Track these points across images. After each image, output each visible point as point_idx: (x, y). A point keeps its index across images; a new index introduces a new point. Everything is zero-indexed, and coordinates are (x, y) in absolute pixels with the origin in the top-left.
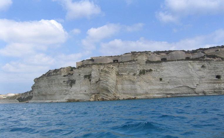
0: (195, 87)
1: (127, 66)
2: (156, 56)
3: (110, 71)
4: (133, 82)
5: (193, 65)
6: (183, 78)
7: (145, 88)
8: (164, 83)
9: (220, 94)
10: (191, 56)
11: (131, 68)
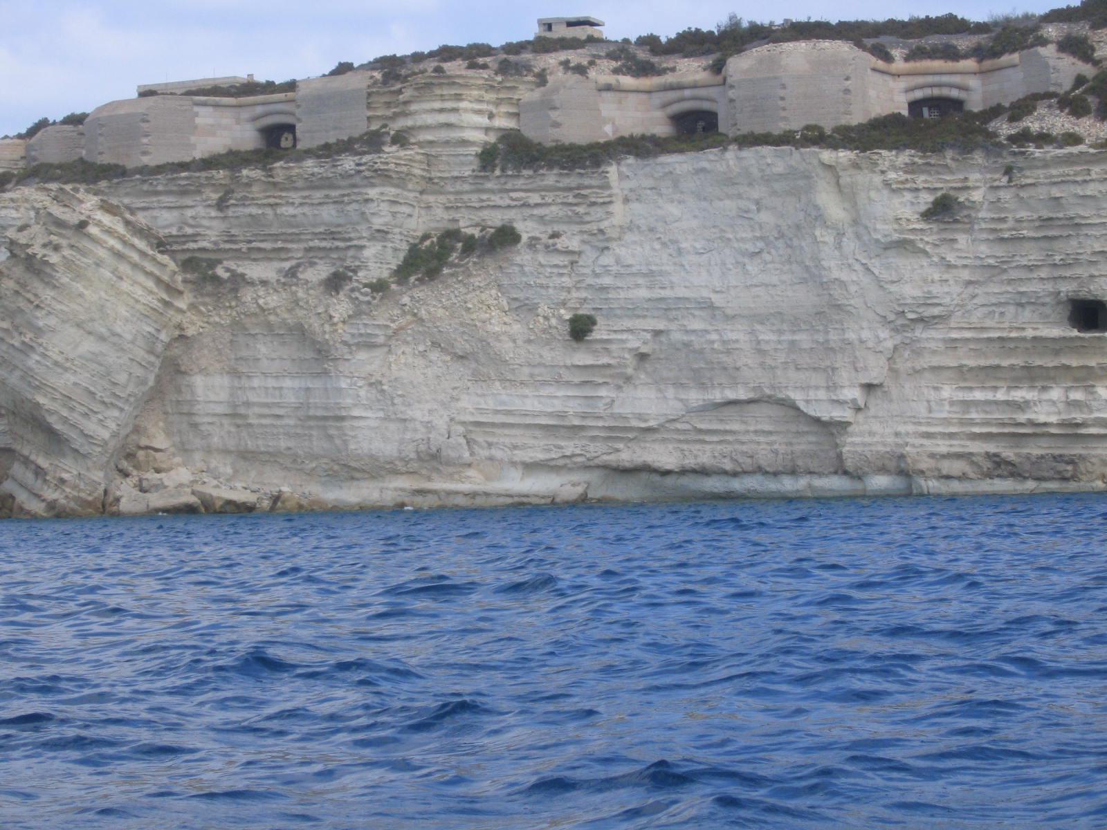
0: (845, 414)
1: (295, 197)
2: (608, 88)
3: (54, 258)
4: (319, 351)
5: (847, 194)
6: (761, 319)
7: (418, 413)
8: (604, 360)
9: (1053, 486)
10: (973, 82)
11: (328, 214)
